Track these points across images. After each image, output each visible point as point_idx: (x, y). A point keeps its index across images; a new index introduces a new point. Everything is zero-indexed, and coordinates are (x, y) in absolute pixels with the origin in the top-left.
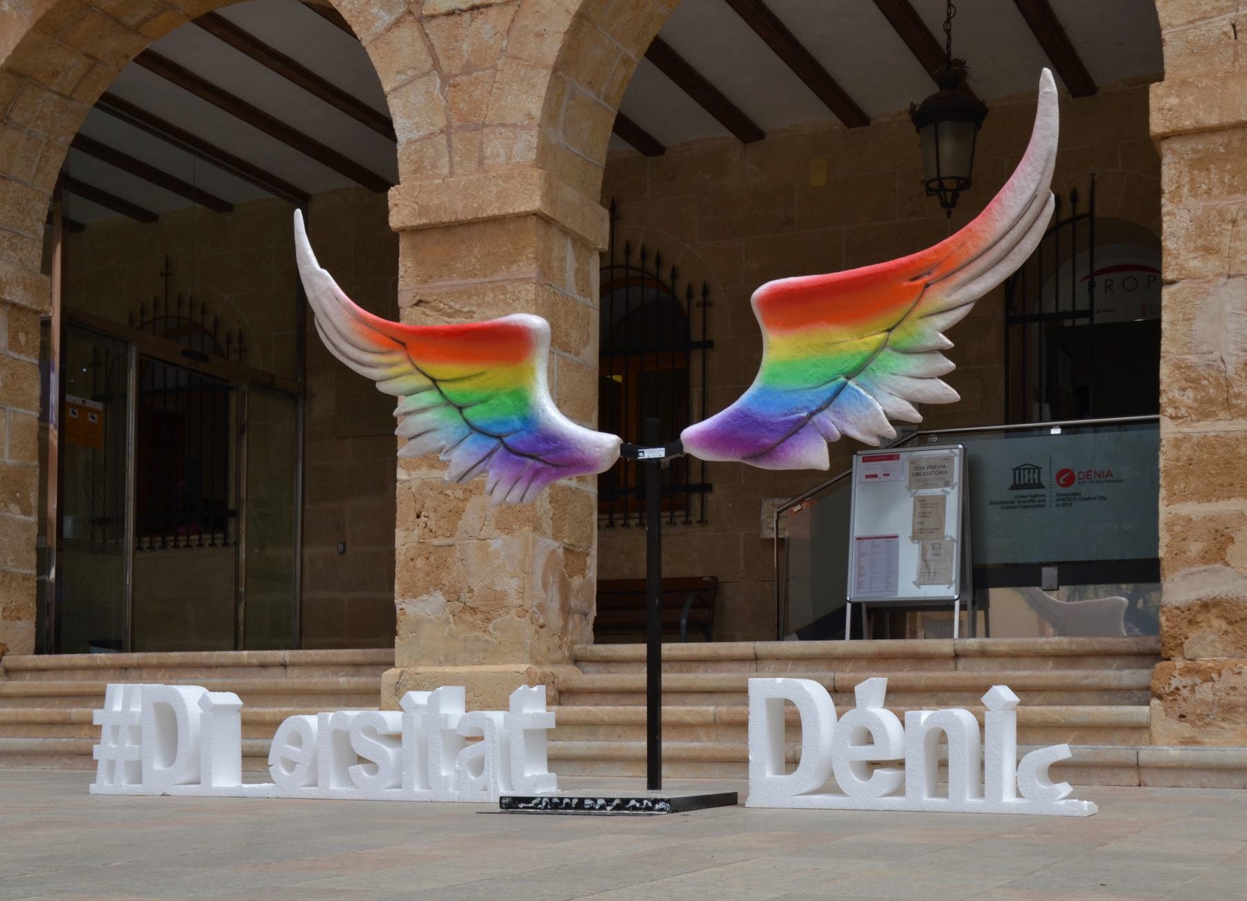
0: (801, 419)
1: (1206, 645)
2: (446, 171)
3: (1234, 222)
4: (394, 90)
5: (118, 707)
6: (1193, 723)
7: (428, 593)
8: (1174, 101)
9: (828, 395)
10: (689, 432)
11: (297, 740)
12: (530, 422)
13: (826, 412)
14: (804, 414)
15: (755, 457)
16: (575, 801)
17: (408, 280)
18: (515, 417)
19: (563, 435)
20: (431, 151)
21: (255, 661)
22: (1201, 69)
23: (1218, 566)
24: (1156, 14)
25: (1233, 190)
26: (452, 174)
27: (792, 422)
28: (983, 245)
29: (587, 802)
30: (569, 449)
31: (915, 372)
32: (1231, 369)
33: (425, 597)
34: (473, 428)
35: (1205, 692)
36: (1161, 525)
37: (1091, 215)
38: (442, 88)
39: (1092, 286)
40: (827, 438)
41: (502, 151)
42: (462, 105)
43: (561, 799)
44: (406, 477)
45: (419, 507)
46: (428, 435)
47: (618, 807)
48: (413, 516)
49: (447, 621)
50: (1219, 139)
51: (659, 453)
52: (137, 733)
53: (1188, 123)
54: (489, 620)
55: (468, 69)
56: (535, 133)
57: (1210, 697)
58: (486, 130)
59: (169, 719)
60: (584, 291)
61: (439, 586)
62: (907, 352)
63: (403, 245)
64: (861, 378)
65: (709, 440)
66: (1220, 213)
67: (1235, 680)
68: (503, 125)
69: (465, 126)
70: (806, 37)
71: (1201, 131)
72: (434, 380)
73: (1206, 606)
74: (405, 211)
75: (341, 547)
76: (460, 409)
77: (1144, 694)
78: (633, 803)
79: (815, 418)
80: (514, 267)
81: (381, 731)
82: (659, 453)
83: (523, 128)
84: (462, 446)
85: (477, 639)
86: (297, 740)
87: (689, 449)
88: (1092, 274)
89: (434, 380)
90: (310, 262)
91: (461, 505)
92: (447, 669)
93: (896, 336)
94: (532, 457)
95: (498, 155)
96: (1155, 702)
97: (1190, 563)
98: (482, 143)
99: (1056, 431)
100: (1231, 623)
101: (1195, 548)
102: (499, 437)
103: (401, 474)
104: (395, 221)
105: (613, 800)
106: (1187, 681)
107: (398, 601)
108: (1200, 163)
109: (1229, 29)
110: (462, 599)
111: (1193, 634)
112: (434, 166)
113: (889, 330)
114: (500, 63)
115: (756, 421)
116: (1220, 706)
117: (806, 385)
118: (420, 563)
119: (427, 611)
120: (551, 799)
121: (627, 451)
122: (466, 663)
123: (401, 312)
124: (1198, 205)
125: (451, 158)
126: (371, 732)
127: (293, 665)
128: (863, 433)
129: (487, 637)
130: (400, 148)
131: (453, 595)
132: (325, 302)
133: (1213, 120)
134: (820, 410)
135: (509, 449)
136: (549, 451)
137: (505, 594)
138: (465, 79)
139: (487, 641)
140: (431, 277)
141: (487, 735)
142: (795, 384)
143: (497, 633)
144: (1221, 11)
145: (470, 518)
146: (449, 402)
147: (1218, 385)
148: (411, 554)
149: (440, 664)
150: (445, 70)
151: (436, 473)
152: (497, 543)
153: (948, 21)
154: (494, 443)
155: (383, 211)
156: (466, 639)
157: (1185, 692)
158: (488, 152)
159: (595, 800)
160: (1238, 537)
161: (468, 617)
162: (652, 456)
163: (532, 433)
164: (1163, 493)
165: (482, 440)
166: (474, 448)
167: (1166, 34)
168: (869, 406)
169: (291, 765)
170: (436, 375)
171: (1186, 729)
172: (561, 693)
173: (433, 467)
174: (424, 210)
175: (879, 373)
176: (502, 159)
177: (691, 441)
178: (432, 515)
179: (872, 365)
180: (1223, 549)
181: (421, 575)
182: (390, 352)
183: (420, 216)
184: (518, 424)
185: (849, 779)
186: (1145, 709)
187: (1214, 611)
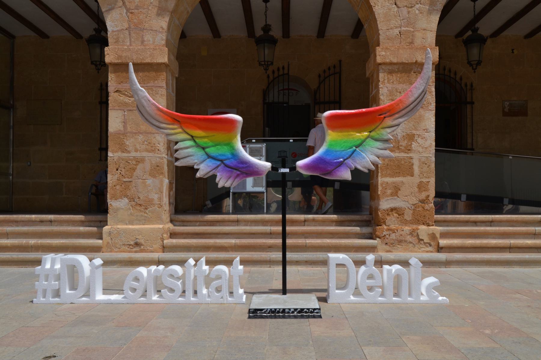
0: (341, 161)
1: (392, 221)
2: (128, 44)
3: (400, 93)
4: (106, 11)
5: (48, 266)
6: (389, 246)
7: (122, 199)
8: (383, 53)
9: (350, 153)
10: (300, 163)
11: (137, 279)
12: (235, 155)
13: (349, 159)
14: (342, 160)
15: (324, 175)
16: (281, 310)
17: (112, 82)
18: (228, 154)
19: (249, 162)
20: (122, 36)
21: (38, 220)
22: (391, 44)
23: (396, 197)
24: (377, 25)
25: (400, 83)
26: (131, 45)
27: (338, 162)
28: (405, 106)
29: (286, 310)
30: (252, 167)
31: (380, 147)
32: (399, 137)
33: (120, 200)
34: (209, 156)
35: (393, 236)
36: (379, 184)
37: (288, 74)
38: (126, 13)
39: (279, 94)
40: (350, 168)
41: (151, 39)
42: (135, 21)
43: (276, 309)
44: (112, 155)
45: (117, 166)
46: (189, 158)
47: (299, 312)
48: (115, 170)
49: (130, 209)
50: (396, 67)
51: (287, 170)
52: (58, 278)
53: (388, 61)
54: (146, 209)
55: (137, 8)
56: (165, 34)
57: (394, 238)
58: (145, 31)
59: (73, 271)
60: (173, 91)
61: (127, 196)
62: (376, 140)
63: (110, 69)
64: (360, 148)
65: (307, 167)
66: (396, 90)
67: (402, 233)
68: (152, 30)
69: (136, 28)
70: (214, 9)
71: (391, 64)
72: (192, 137)
73: (392, 210)
74: (112, 57)
75: (29, 163)
76: (203, 148)
77: (371, 237)
78: (305, 310)
79: (346, 161)
80: (156, 82)
81: (176, 276)
82: (287, 170)
83: (160, 32)
84: (205, 163)
85: (142, 216)
86: (137, 279)
87: (298, 169)
88: (279, 91)
89: (192, 137)
90: (136, 85)
91: (135, 166)
92: (130, 227)
93: (373, 134)
94: (236, 169)
95: (150, 41)
96: (377, 239)
97: (387, 196)
98: (143, 35)
99: (291, 141)
100: (399, 215)
101: (389, 192)
102: (222, 161)
103: (110, 154)
104: (107, 60)
105: (297, 309)
106: (388, 233)
107: (109, 201)
108: (391, 72)
109: (398, 33)
110: (136, 201)
111: (388, 218)
112: (123, 41)
113: (370, 132)
114: (150, 8)
115: (325, 161)
116: (398, 240)
117: (343, 149)
118: (118, 187)
119: (121, 205)
120: (271, 309)
121: (274, 169)
122: (137, 224)
123: (110, 94)
124: (390, 86)
125: (130, 40)
126: (172, 276)
127: (55, 221)
128: (363, 167)
129: (146, 215)
130: (109, 33)
131: (131, 199)
132: (143, 101)
133: (395, 61)
134: (347, 159)
135: (226, 166)
136: (243, 168)
137: (153, 200)
138: (136, 11)
139: (146, 217)
140: (122, 82)
141: (223, 277)
142: (338, 148)
143: (150, 214)
144: (396, 27)
145: (139, 171)
146: (198, 146)
147: (395, 142)
148: (114, 184)
149: (127, 225)
150: (128, 7)
151: (125, 155)
152: (149, 182)
153: (266, 12)
154: (219, 163)
155: (102, 55)
156: (137, 216)
157: (387, 236)
158: (146, 39)
159: (290, 309)
160: (401, 189)
161: (138, 208)
162: (284, 171)
163: (236, 160)
164: (380, 174)
165: (214, 161)
166: (210, 164)
167: (381, 32)
168: (364, 158)
169: (134, 290)
170: (194, 134)
171: (387, 247)
172: (171, 234)
173: (124, 152)
174: (120, 57)
175: (367, 147)
176: (151, 42)
177: (301, 167)
178: (123, 170)
179: (364, 143)
180: (397, 192)
181: (118, 192)
182: (172, 124)
183: (118, 59)
184: (230, 156)
185: (363, 290)
186: (376, 241)
187: (394, 211)
